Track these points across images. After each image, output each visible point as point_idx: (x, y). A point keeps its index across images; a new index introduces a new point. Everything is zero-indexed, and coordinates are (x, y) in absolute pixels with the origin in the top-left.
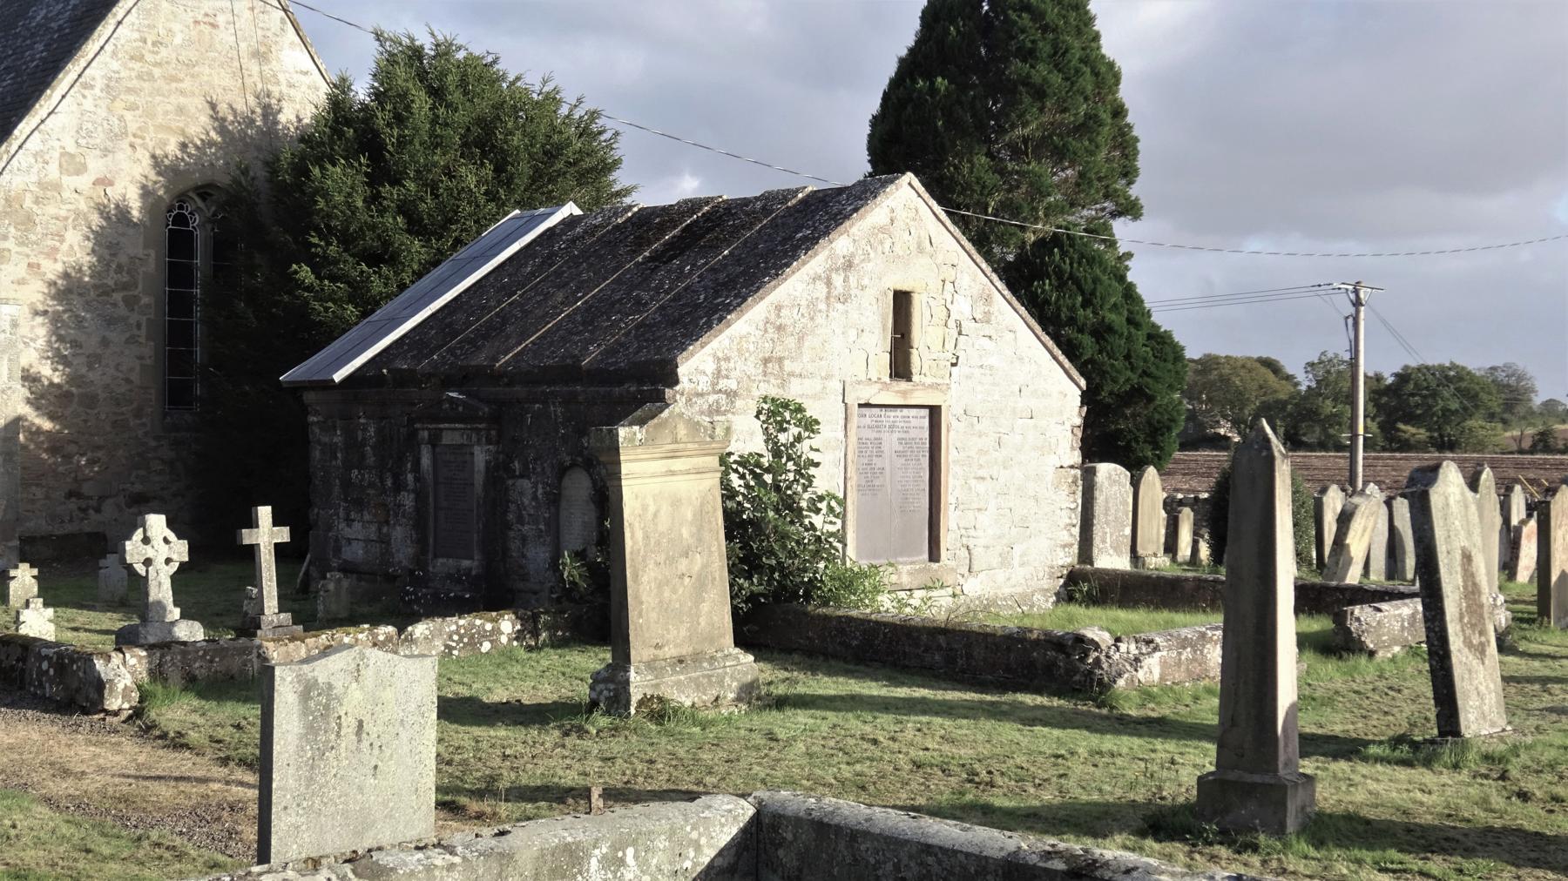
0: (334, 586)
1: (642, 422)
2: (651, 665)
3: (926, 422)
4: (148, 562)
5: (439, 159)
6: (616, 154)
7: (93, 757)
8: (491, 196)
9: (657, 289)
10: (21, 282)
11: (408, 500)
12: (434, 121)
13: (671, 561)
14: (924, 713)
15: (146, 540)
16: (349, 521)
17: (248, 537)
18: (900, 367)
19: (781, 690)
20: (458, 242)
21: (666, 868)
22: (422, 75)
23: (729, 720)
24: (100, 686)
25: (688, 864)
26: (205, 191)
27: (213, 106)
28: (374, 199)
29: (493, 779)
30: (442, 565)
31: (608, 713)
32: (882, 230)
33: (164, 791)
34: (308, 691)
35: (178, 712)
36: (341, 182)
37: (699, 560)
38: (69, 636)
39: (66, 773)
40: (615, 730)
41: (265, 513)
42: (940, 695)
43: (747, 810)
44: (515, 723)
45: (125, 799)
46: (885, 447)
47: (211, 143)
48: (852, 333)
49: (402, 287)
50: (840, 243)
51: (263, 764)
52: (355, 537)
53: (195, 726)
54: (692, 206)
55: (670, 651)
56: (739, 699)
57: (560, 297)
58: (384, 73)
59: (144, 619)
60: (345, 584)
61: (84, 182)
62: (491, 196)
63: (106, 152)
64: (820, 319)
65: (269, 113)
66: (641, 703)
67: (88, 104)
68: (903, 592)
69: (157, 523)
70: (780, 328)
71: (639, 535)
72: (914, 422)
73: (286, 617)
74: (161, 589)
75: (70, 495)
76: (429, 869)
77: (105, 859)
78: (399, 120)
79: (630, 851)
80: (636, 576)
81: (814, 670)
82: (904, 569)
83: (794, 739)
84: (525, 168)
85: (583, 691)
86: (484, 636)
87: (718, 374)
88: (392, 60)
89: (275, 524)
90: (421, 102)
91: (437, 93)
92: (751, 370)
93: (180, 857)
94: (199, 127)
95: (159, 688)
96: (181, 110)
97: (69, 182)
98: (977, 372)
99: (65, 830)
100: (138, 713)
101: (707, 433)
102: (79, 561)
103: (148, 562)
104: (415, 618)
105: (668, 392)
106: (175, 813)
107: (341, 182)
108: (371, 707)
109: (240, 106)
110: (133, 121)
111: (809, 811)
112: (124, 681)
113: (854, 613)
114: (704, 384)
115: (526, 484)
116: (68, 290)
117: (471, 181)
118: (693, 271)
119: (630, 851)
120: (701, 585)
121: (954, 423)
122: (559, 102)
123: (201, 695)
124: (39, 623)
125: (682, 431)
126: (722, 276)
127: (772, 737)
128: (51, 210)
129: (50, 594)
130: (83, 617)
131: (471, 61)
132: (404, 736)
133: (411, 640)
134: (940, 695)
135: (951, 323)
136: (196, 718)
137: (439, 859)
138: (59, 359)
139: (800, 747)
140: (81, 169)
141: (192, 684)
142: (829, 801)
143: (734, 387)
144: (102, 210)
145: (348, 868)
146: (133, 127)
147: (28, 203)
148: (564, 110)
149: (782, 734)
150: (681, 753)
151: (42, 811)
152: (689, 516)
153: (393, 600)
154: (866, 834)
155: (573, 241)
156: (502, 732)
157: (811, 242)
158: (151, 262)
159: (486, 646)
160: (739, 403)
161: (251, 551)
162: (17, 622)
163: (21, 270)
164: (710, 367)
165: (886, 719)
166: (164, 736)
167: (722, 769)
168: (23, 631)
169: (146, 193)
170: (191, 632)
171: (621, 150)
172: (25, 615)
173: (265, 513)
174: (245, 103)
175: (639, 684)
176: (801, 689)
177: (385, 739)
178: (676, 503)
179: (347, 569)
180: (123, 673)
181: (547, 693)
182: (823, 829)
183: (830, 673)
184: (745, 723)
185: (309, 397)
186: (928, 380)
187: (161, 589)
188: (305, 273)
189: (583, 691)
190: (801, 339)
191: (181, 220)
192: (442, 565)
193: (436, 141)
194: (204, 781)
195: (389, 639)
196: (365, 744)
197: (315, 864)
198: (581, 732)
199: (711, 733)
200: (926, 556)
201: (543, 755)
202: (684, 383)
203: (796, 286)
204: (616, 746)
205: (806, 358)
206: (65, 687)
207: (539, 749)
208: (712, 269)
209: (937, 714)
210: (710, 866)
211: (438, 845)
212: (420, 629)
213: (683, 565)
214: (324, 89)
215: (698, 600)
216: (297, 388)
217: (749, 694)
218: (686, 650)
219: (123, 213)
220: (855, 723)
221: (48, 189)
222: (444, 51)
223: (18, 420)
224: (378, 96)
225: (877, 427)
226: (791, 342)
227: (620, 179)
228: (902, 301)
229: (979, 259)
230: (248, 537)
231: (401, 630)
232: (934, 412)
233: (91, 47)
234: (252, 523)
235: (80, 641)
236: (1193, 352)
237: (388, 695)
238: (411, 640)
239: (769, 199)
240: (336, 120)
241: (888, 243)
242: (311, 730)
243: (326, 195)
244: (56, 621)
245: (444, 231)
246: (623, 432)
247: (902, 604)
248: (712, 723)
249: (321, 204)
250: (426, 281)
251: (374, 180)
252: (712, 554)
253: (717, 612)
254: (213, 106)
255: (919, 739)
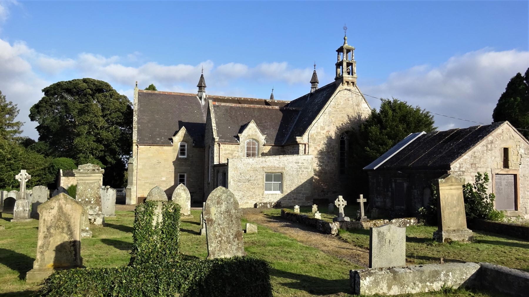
0: (375, 211)
1: (444, 178)
2: (447, 231)
3: (513, 178)
4: (339, 205)
5: (394, 124)
6: (433, 120)
7: (330, 243)
8: (405, 131)
9: (445, 149)
10: (313, 151)
11: (390, 194)
12: (393, 116)
13: (451, 208)
14: (517, 246)
15: (339, 201)
16: (377, 198)
17: (358, 201)
18: (506, 165)
19: (479, 239)
20: (399, 141)
21: (459, 278)
22: (391, 107)
23: (467, 244)
24: (330, 229)
25: (464, 277)
26: (347, 132)
27: (348, 116)
28: (381, 133)
29: (412, 254)
30: (397, 207)
31: (437, 241)
32: (500, 134)
33: (344, 251)
34: (379, 233)
35: (345, 235)
36: (374, 129)
37: (458, 209)
38: (323, 219)
39: (325, 246)
40: (439, 245)
41: (361, 196)
42: (521, 242)
43: (478, 267)
44: (416, 242)
45: (337, 252)
46: (503, 184)
47: (348, 123)
48: (493, 158)
49: (387, 150)
50: (490, 138)
51: (370, 249)
52: (379, 201)
53: (349, 238)
54: (452, 131)
55: (452, 228)
56: (469, 240)
57: (422, 151)
58: (383, 107)
59: (338, 216)
60: (377, 210)
61: (325, 132)
62: (405, 131)
63: (329, 126)
64: (485, 155)
65: (359, 116)
66: (445, 239)
67: (325, 117)
68: (509, 217)
69: (341, 197)
70: (475, 157)
71: (444, 202)
72: (510, 178)
73: (366, 217)
74: (342, 211)
75: (322, 191)
76: (406, 272)
77: (335, 263)
78: (386, 116)
79: (450, 273)
80: (443, 212)
81: (487, 235)
82: (509, 212)
83: (484, 250)
84: (413, 125)
85: (431, 236)
86: (408, 223)
87: (460, 167)
88: (384, 104)
89: (364, 198)
90: (390, 112)
91: (394, 110)
92: (468, 166)
93: (349, 264)
94: (346, 120)
95: (342, 230)
96: (342, 117)
97: (322, 132)
98: (526, 166)
99: (327, 257)
100: (338, 235)
101: (459, 179)
102: (326, 205)
103: (339, 205)
104: (393, 219)
105: (448, 171)
106: (347, 255)
107: (374, 129)
108: (392, 237)
109: (354, 116)
110: (333, 120)
111: (494, 268)
112: (335, 228)
113: (497, 222)
114: (457, 169)
115: (415, 191)
116: (321, 153)
117: (401, 129)
118: (453, 145)
119: (450, 273)
120: (459, 214)
121: (521, 178)
122: (420, 110)
123: (350, 232)
124: (318, 216)
125: (453, 180)
126: (460, 146)
127: (478, 249)
128: (319, 137)
129: (320, 210)
130: (325, 215)
131: (401, 103)
132: (399, 244)
133: (392, 223)
134: (521, 242)
135: (519, 155)
136: (349, 236)
137: (408, 271)
138: (320, 166)
139: (486, 252)
140: (324, 129)
141: (348, 230)
142: (500, 266)
143: (464, 170)
144: (327, 137)
145: (388, 271)
146: (333, 121)
147: (315, 136)
148: (421, 112)
149: (480, 249)
150: (456, 251)
151: (322, 253)
152: (456, 198)
153: (388, 214)
154: (510, 275)
155: (424, 139)
156: (413, 244)
157: (482, 138)
158: (337, 146)
159: (408, 225)
160: (465, 174)
161: (359, 203)
162: (314, 215)
163: (313, 149)
164: (458, 166)
165: (507, 247)
166: (343, 240)
167: (467, 256)
168: (315, 217)
169: (336, 133)
170: (347, 219)
171: (434, 119)
172: (316, 214)
173: (361, 196)
174: (355, 115)
175: (445, 235)
176: (484, 239)
177: (395, 244)
178: (452, 196)
179: (377, 207)
180: (335, 227)
181: (422, 236)
182: (498, 273)
183: (491, 235)
184: (471, 246)
185: (369, 172)
186: (513, 168)
187: (342, 211)
188: (368, 149)
189: (431, 236)
190: (480, 159)
191: (342, 138)
192: (397, 207)
193: (395, 119)
194: (352, 249)
195: (387, 222)
196: (391, 245)
197: (381, 269)
198: (432, 245)
199: (463, 247)
200: (514, 209)
201: (423, 250)
202: (452, 169)
203: (479, 148)
204: (440, 249)
205: (482, 163)
206: (322, 228)
207: (422, 248)
208: (458, 144)
209: (521, 247)
210: (470, 278)
211: (407, 268)
212: (394, 221)
213: (454, 209)
214: (370, 111)
215: (458, 218)
216: (366, 171)
217: (471, 239)
218: (455, 228)
219: (331, 138)
220: (499, 248)
221: (318, 133)
222: (395, 101)
223: (313, 177)
224: (382, 112)
225: (500, 179)
226: (478, 160)
227: (434, 126)
228: (506, 150)
229: (526, 140)
230: (358, 201)
231: (390, 221)
232: (515, 176)
233: (326, 106)
234: (359, 198)
235: (326, 220)
236: (39, 136)
237: (395, 235)
238: (392, 223)
239: (471, 129)
240: (373, 117)
241: (502, 138)
242: (380, 241)
243: (371, 132)
244: (321, 215)
245: (397, 139)
246: (439, 180)
247: (509, 220)
248: (463, 245)
249: (370, 134)
250: (392, 149)
251: (381, 129)
252: (461, 208)
253: (462, 220)
254: (348, 116)
255: (516, 252)
